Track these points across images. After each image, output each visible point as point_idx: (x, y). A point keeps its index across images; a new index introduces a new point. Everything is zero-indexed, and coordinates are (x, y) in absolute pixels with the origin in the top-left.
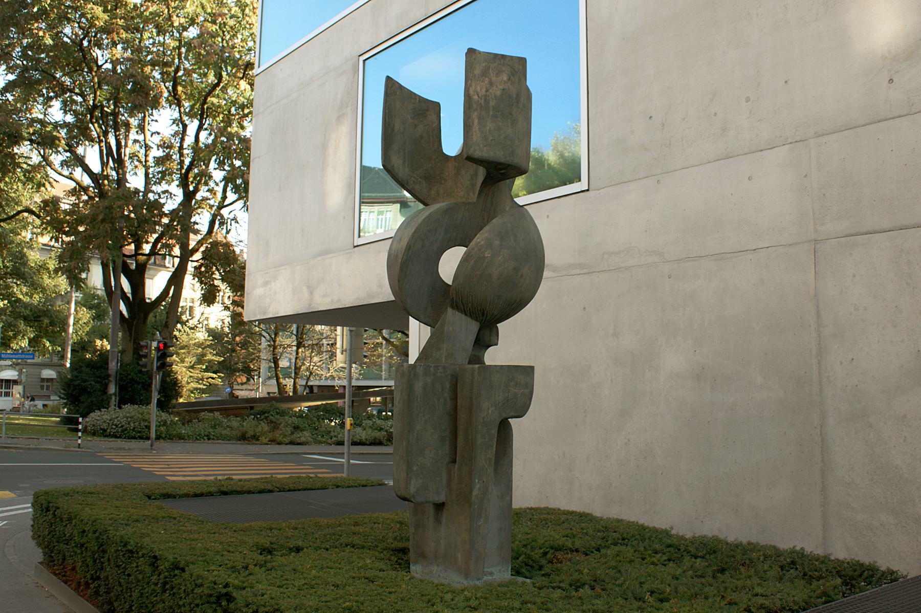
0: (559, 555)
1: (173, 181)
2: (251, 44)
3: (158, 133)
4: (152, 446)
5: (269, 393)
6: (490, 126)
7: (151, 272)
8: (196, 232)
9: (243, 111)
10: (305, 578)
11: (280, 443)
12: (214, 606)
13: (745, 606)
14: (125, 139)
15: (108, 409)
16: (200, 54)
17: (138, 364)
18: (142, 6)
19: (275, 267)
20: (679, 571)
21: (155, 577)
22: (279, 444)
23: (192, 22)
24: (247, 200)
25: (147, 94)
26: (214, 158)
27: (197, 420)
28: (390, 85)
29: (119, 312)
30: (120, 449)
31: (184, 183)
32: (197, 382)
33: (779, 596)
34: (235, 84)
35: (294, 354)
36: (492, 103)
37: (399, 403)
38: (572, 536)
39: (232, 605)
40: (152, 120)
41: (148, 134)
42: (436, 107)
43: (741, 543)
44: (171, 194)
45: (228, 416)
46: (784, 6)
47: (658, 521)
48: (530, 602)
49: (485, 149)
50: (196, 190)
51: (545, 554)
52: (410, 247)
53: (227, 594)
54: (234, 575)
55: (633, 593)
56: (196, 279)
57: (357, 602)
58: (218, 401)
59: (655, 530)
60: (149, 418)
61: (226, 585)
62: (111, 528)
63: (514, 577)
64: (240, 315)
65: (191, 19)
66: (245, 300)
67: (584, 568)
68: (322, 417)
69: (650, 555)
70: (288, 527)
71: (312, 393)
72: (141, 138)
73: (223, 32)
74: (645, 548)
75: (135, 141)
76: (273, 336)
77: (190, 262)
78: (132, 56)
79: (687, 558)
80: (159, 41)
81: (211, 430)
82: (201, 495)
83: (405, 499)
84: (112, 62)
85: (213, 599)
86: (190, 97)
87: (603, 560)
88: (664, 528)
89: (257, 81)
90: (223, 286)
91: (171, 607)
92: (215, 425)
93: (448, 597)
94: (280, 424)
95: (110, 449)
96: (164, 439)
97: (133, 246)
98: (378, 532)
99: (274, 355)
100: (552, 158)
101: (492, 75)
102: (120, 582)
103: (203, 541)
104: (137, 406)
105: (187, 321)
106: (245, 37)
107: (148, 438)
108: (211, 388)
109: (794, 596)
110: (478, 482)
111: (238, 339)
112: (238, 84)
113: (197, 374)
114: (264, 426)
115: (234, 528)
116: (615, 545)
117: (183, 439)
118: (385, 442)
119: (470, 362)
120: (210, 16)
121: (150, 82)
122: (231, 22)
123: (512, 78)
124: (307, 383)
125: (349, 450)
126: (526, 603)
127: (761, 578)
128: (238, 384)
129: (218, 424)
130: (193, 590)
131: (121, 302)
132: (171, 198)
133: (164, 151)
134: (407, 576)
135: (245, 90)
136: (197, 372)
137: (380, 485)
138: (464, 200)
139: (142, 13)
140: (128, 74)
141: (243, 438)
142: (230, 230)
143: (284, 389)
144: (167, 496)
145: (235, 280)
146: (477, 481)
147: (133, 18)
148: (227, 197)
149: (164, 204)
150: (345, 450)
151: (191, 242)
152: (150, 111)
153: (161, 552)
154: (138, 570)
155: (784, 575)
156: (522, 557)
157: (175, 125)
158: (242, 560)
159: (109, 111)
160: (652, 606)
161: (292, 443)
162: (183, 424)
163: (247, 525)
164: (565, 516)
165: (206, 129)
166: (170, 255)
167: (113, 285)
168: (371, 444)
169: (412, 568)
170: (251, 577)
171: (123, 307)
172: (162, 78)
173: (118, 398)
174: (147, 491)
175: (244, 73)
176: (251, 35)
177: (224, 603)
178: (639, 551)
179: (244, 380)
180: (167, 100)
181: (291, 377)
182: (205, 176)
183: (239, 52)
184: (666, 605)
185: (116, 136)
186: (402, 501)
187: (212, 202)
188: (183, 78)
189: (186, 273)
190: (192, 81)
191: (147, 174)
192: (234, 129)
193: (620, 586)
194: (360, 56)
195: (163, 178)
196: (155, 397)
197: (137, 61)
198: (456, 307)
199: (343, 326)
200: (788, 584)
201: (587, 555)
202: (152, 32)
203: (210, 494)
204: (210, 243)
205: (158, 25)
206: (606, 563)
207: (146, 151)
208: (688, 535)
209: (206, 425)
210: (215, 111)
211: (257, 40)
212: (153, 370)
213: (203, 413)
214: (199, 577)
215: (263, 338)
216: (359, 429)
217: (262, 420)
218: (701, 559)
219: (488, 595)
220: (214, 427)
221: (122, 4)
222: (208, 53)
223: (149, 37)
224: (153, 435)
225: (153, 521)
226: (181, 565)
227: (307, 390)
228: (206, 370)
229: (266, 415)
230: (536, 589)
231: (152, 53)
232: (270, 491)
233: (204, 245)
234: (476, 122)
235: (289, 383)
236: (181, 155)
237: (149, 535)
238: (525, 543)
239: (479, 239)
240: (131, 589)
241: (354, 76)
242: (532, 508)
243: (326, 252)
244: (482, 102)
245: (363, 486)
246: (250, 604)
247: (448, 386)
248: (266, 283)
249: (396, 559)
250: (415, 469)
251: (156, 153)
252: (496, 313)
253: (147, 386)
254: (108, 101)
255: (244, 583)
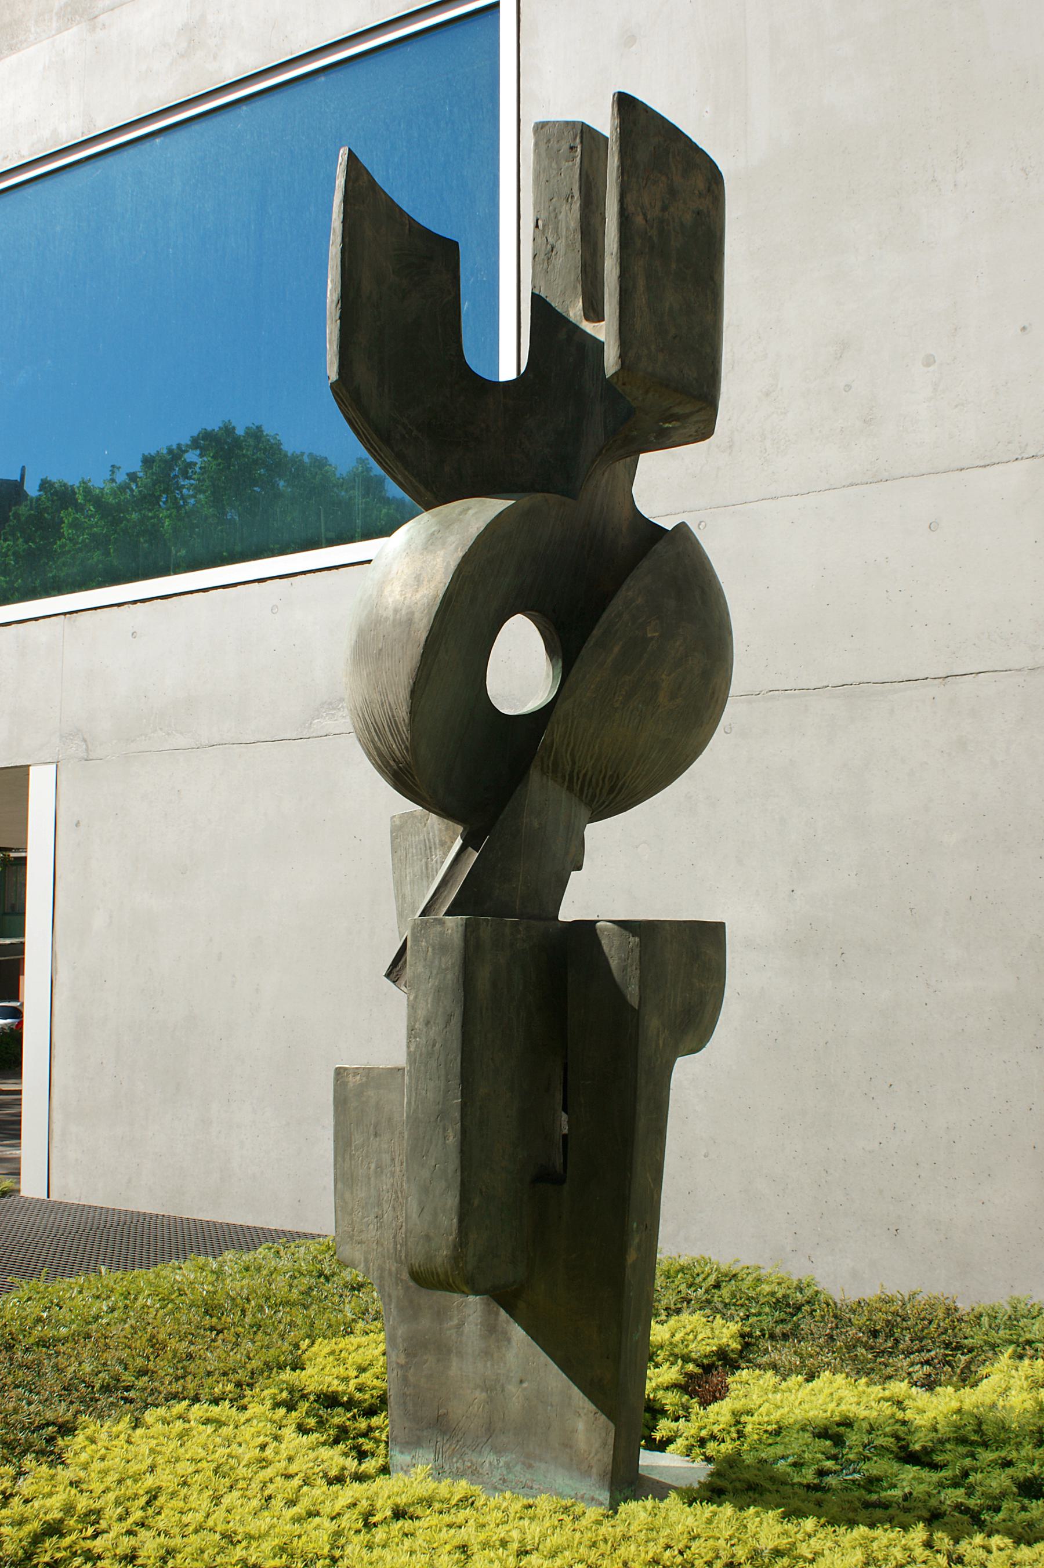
37: (427, 1023)
101: (674, 169)
146: (635, 1225)
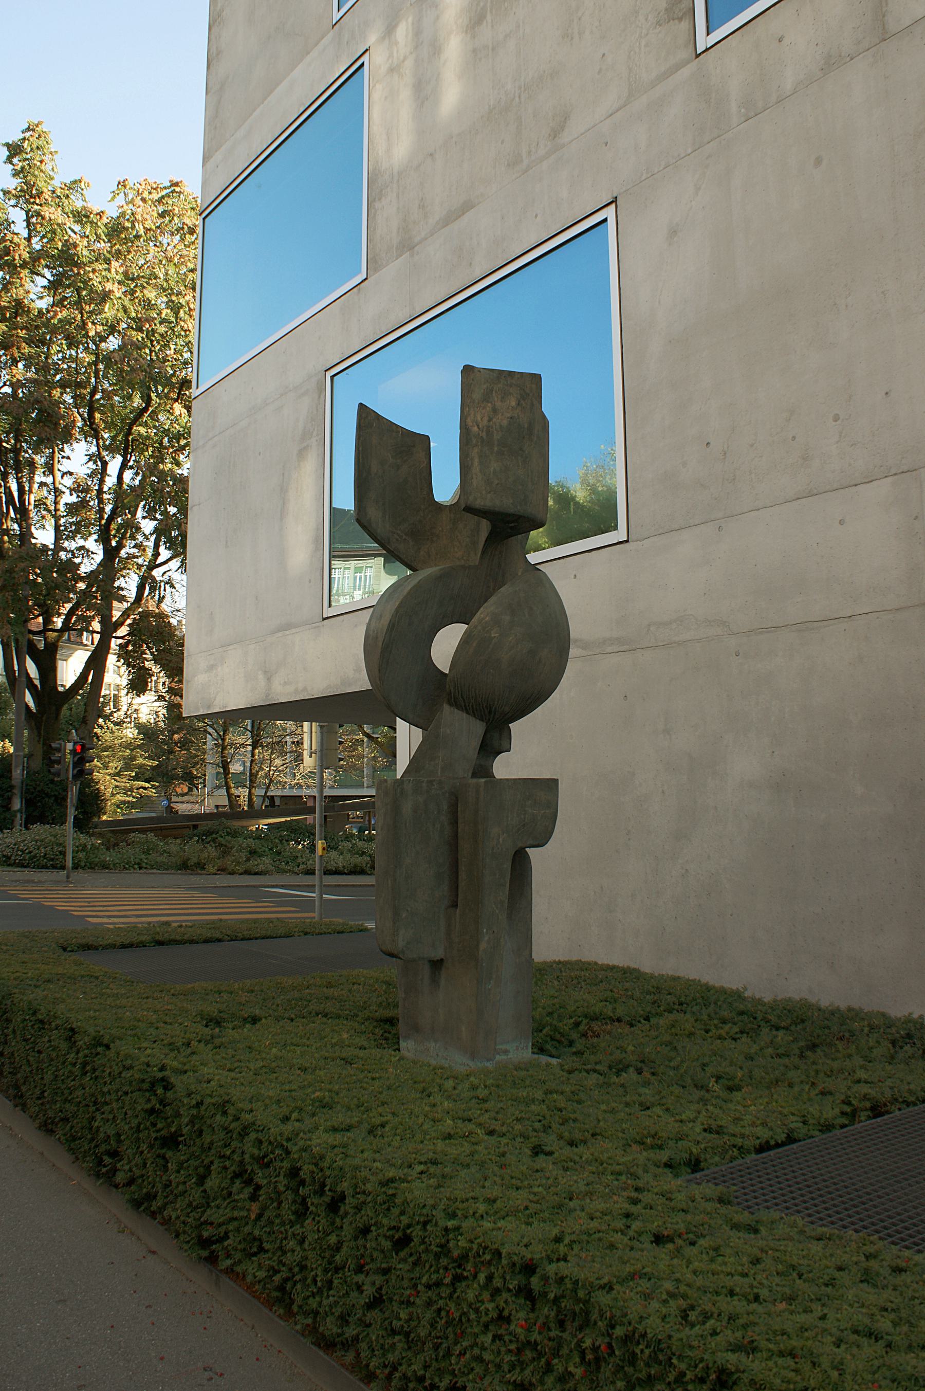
0: (596, 1026)
1: (90, 534)
2: (187, 355)
3: (71, 474)
4: (68, 877)
5: (217, 807)
6: (495, 466)
7: (65, 651)
8: (122, 599)
9: (178, 443)
10: (263, 1059)
11: (232, 873)
12: (147, 1094)
13: (843, 1097)
14: (30, 483)
15: (11, 829)
16: (122, 370)
17: (49, 771)
18: (48, 311)
19: (222, 647)
20: (755, 1048)
21: (73, 1055)
22: (230, 874)
23: (112, 329)
24: (185, 556)
25: (57, 424)
26: (142, 504)
27: (124, 844)
28: (364, 416)
29: (24, 706)
30: (28, 881)
31: (104, 538)
32: (125, 794)
33: (889, 1082)
34: (168, 407)
35: (249, 756)
36: (497, 436)
38: (612, 1001)
39: (169, 1094)
40: (63, 457)
41: (58, 475)
42: (426, 440)
43: (838, 1009)
44: (88, 551)
45: (165, 837)
46: (883, 292)
47: (729, 980)
48: (556, 1092)
49: (489, 495)
50: (120, 546)
51: (577, 1024)
52: (394, 625)
53: (163, 1079)
54: (173, 1054)
55: (692, 1079)
56: (122, 661)
57: (330, 1091)
58: (153, 817)
59: (723, 991)
60: (64, 842)
61: (163, 1068)
62: (17, 991)
63: (536, 1056)
64: (179, 706)
65: (109, 327)
66: (184, 686)
67: (628, 1044)
68: (286, 838)
69: (716, 1027)
70: (242, 990)
71: (273, 806)
72: (49, 480)
73: (152, 341)
74: (709, 1016)
75: (42, 484)
76: (221, 733)
77: (113, 640)
78: (36, 377)
79: (765, 1030)
80: (70, 355)
81: (143, 856)
82: (131, 945)
83: (392, 955)
84: (12, 385)
85: (146, 1086)
86: (109, 426)
87: (653, 1033)
88: (734, 988)
89: (195, 405)
90: (155, 669)
91: (93, 1095)
92: (148, 850)
93: (450, 1084)
94: (232, 848)
95: (16, 881)
96: (83, 868)
97: (40, 619)
98: (358, 995)
99: (222, 757)
100: (581, 495)
102: (28, 1061)
103: (133, 1009)
104: (48, 826)
105: (111, 714)
106: (179, 347)
107: (63, 868)
108: (143, 802)
109: (909, 1083)
110: (487, 933)
111: (176, 737)
112: (172, 408)
113: (124, 782)
114: (212, 851)
115: (172, 991)
116: (670, 1011)
117: (107, 868)
118: (368, 870)
119: (474, 775)
120: (135, 322)
121: (60, 408)
122: (162, 329)
123: (522, 402)
124: (266, 793)
125: (321, 881)
126: (551, 1093)
127: (865, 1057)
128: (178, 795)
129: (153, 849)
130: (120, 1073)
131: (27, 691)
132: (89, 556)
133: (78, 496)
134: (395, 1056)
135: (180, 415)
136: (125, 780)
137: (361, 931)
138: (463, 562)
139: (49, 320)
140: (32, 399)
141: (184, 866)
142: (164, 597)
143: (237, 801)
144: (87, 947)
145: (170, 661)
147: (37, 327)
148: (159, 554)
149: (80, 564)
150: (317, 883)
151: (114, 612)
152: (60, 447)
153: (79, 1024)
154: (51, 1046)
155: (896, 1052)
156: (547, 1029)
157: (91, 463)
158: (182, 1034)
159: (8, 446)
160: (718, 1097)
161: (247, 872)
162: (108, 849)
163: (190, 986)
164: (603, 972)
165: (131, 468)
166: (88, 631)
167: (16, 668)
168: (351, 873)
169: (403, 1044)
170: (194, 1057)
171: (29, 699)
172: (75, 402)
173: (24, 816)
174: (61, 941)
175: (179, 394)
176: (187, 344)
177: (160, 1091)
178: (701, 1020)
179: (186, 790)
180: (82, 430)
181: (245, 786)
182: (132, 528)
183: (172, 367)
184: (737, 1096)
185: (18, 479)
186: (384, 956)
187: (140, 561)
188: (102, 402)
189: (108, 653)
190: (112, 406)
191: (57, 528)
192: (168, 466)
193: (676, 1068)
194: (366, 279)
195: (77, 531)
196: (71, 813)
197: (43, 383)
198: (454, 703)
199: (311, 721)
200: (902, 1066)
201: (632, 1025)
202: (62, 344)
203: (142, 945)
204: (140, 613)
205: (69, 335)
206: (657, 1037)
207: (56, 497)
208: (768, 998)
209: (137, 850)
210: (142, 443)
211: (195, 350)
212: (68, 779)
213: (133, 835)
214: (127, 1056)
215: (208, 736)
216: (333, 854)
217: (208, 843)
218: (785, 1031)
219: (501, 1082)
220: (147, 852)
221: (24, 311)
222: (133, 370)
223: (57, 351)
224: (69, 863)
225: (69, 981)
226: (105, 1042)
227: (267, 802)
228: (136, 778)
229: (214, 836)
230: (565, 1074)
231: (63, 370)
232: (219, 940)
233: (132, 617)
234: (476, 461)
235: (243, 793)
236: (101, 501)
237: (63, 1001)
238: (550, 1010)
239: (483, 614)
240: (42, 1070)
241: (319, 397)
242: (560, 962)
243: (288, 626)
244: (484, 435)
245: (338, 933)
246: (193, 1093)
247: (445, 807)
248: (211, 668)
249: (381, 1032)
250: (404, 915)
251: (68, 498)
252: (507, 709)
253: (61, 800)
254: (8, 433)
255: (185, 1064)
